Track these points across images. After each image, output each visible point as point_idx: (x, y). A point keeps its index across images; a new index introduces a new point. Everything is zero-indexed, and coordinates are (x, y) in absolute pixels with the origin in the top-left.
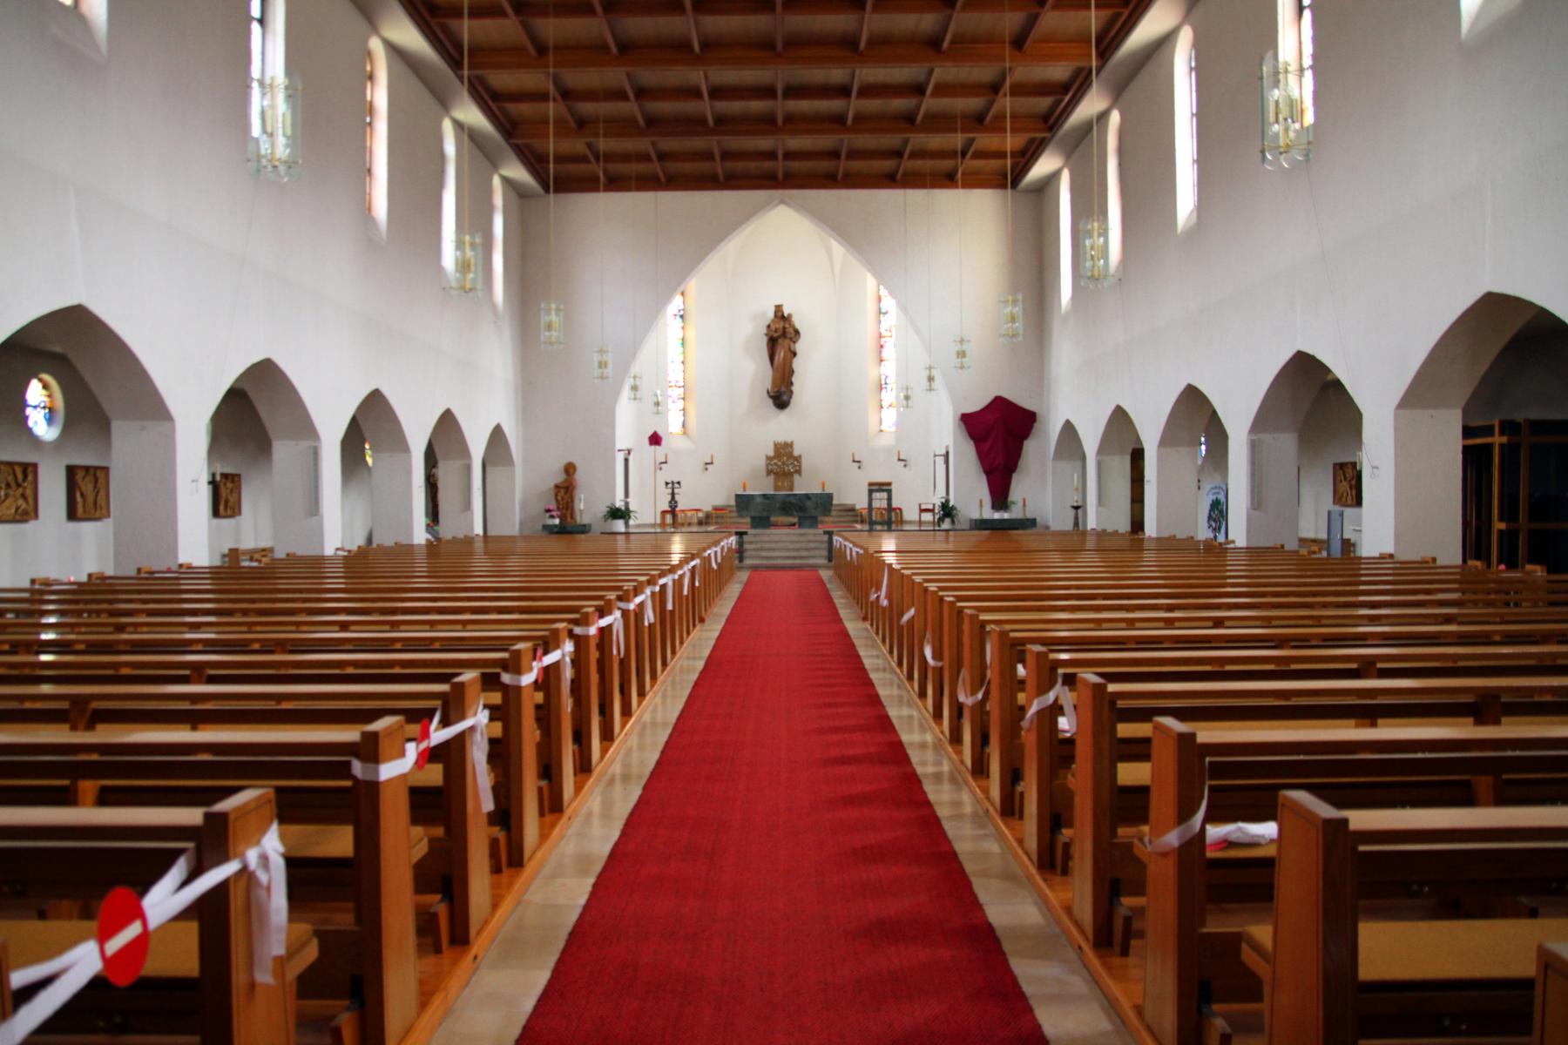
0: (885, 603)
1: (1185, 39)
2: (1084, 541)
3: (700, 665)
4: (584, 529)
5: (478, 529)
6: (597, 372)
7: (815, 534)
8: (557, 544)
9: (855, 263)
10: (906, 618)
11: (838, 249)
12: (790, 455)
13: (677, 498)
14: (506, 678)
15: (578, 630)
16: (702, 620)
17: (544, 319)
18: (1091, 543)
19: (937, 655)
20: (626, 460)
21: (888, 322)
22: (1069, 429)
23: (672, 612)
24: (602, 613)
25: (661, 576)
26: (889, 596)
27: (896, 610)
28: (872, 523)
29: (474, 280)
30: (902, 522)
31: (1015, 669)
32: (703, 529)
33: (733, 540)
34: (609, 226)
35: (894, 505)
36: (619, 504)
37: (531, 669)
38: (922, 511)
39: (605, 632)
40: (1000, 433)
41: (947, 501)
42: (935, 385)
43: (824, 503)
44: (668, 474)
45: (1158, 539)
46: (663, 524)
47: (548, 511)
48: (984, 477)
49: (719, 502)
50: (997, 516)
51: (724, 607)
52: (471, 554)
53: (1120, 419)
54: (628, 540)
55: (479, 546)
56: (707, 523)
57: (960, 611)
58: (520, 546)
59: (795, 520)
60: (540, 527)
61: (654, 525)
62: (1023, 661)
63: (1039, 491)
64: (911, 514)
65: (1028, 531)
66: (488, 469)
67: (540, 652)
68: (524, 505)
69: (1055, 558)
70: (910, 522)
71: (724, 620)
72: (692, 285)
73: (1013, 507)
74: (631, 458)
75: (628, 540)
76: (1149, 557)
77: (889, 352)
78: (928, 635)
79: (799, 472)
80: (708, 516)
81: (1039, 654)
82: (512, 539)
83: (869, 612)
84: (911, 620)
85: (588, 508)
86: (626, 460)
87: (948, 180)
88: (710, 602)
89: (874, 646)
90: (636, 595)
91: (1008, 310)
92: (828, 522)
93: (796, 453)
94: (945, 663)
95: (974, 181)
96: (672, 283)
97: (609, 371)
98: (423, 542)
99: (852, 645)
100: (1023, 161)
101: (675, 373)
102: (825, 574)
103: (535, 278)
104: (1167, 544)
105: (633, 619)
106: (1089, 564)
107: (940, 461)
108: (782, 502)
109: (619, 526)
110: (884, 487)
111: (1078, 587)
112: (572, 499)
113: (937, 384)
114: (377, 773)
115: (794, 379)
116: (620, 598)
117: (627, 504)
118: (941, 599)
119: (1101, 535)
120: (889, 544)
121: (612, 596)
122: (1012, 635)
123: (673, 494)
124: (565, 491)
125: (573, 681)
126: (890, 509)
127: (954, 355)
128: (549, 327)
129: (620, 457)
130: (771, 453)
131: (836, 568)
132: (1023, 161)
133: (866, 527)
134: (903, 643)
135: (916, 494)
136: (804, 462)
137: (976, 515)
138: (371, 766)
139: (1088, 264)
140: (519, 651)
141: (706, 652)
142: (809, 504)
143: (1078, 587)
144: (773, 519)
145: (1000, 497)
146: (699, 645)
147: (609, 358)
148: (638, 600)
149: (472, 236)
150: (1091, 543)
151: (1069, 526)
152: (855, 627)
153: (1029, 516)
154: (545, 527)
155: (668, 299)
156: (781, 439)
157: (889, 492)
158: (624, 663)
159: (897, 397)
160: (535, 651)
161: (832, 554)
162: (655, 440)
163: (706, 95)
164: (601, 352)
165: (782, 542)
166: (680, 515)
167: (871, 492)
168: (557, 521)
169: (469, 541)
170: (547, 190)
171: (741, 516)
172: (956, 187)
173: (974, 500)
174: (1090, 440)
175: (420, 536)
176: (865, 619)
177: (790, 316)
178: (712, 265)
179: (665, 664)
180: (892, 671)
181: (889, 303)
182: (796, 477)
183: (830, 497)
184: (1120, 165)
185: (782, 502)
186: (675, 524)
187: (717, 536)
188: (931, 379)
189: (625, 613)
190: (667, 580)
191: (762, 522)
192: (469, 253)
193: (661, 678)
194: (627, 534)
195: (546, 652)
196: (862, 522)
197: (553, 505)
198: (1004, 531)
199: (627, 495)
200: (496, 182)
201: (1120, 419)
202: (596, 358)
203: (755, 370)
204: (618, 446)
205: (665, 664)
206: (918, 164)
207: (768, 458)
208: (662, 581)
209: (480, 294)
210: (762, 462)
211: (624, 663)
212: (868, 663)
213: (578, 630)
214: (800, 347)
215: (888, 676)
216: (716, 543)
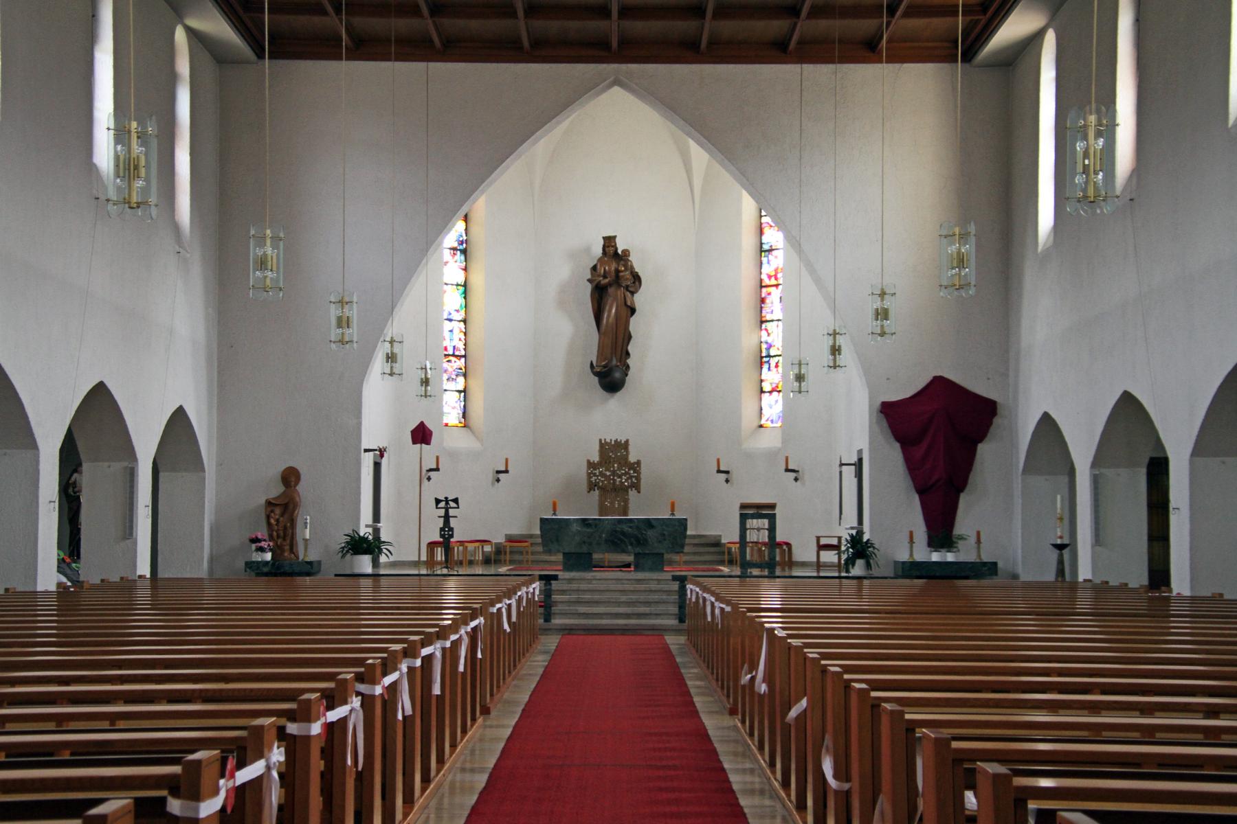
0: (763, 688)
1: (1050, 39)
2: (1073, 599)
3: (481, 780)
4: (310, 569)
5: (144, 568)
6: (335, 333)
7: (660, 580)
8: (265, 591)
9: (725, 178)
10: (793, 713)
11: (699, 155)
12: (624, 461)
13: (453, 522)
14: (175, 806)
15: (292, 728)
16: (486, 711)
17: (255, 252)
18: (1084, 602)
19: (842, 772)
20: (377, 466)
21: (774, 262)
22: (1047, 424)
23: (440, 698)
24: (332, 700)
25: (424, 644)
26: (768, 679)
27: (779, 701)
28: (745, 565)
29: (145, 191)
30: (791, 564)
31: (962, 799)
32: (492, 570)
33: (536, 586)
34: (355, 110)
35: (778, 539)
36: (364, 531)
37: (216, 792)
38: (822, 547)
39: (335, 730)
40: (940, 432)
41: (860, 533)
42: (842, 359)
43: (673, 533)
44: (439, 487)
45: (1193, 599)
46: (431, 563)
47: (255, 540)
48: (916, 499)
49: (515, 531)
50: (935, 557)
51: (518, 693)
52: (130, 606)
53: (1128, 409)
54: (376, 587)
55: (143, 595)
56: (498, 562)
57: (876, 705)
58: (209, 595)
59: (630, 558)
60: (241, 564)
61: (416, 564)
62: (972, 787)
63: (1000, 519)
64: (804, 552)
65: (985, 582)
66: (163, 476)
67: (230, 765)
68: (216, 530)
69: (1028, 624)
70: (803, 564)
71: (519, 710)
72: (480, 205)
73: (961, 544)
74: (384, 462)
75: (376, 587)
76: (1180, 627)
77: (774, 308)
78: (828, 740)
79: (636, 486)
80: (499, 550)
81: (996, 776)
82: (196, 583)
83: (738, 701)
84: (803, 715)
85: (316, 536)
86: (377, 466)
87: (867, 50)
88: (497, 686)
89: (746, 754)
90: (385, 674)
91: (953, 249)
92: (679, 564)
93: (632, 459)
94: (854, 785)
95: (907, 51)
96: (454, 202)
97: (353, 332)
98: (53, 588)
99: (714, 753)
100: (983, 19)
101: (453, 337)
102: (674, 642)
103: (244, 197)
104: (1208, 608)
105: (379, 711)
106: (1082, 635)
107: (849, 472)
108: (611, 528)
109: (364, 564)
110: (765, 511)
111: (1060, 673)
112: (293, 522)
113: (847, 357)
114: (197, 810)
115: (631, 348)
116: (360, 678)
117: (377, 531)
118: (847, 685)
119: (1100, 589)
120: (771, 596)
121: (348, 674)
122: (955, 745)
123: (447, 517)
124: (282, 510)
125: (281, 808)
126: (773, 543)
127: (870, 314)
128: (262, 264)
129: (368, 461)
130: (596, 458)
131: (689, 633)
132: (983, 19)
133: (737, 571)
134: (791, 750)
135: (814, 521)
136: (644, 470)
137: (904, 556)
138: (193, 804)
139: (1079, 179)
140: (198, 763)
141: (491, 763)
142: (650, 533)
143: (1060, 673)
144: (596, 556)
145: (941, 529)
146: (484, 744)
147: (353, 313)
148: (388, 680)
149: (141, 123)
150: (1084, 602)
151: (1050, 576)
152: (716, 724)
153: (986, 558)
154: (250, 565)
155: (443, 226)
156: (610, 437)
157: (772, 519)
158: (363, 779)
159: (784, 377)
160: (224, 761)
161: (685, 611)
162: (421, 435)
163: (521, 13)
164: (342, 303)
165: (610, 592)
166: (457, 551)
167: (743, 518)
168: (268, 556)
169: (128, 585)
170: (260, 55)
171: (549, 552)
172: (881, 62)
173: (902, 533)
174: (1082, 448)
175: (48, 578)
176: (733, 712)
177: (626, 253)
178: (510, 177)
179: (426, 780)
180: (774, 795)
181: (773, 237)
182: (632, 493)
183: (683, 523)
184: (1138, 21)
185: (611, 528)
186: (448, 563)
187: (513, 581)
188: (835, 350)
189: (367, 701)
190: (433, 649)
191: (580, 561)
192: (137, 149)
193: (419, 802)
194: (375, 576)
195: (241, 765)
196: (731, 562)
197: (262, 533)
198: (947, 582)
199: (376, 516)
200: (180, 35)
201: (1128, 409)
202: (334, 312)
203: (570, 333)
204: (365, 445)
205: (426, 780)
206: (823, 25)
207: (590, 465)
208: (425, 651)
209: (154, 211)
210: (583, 471)
211: (363, 779)
212: (736, 781)
213: (292, 728)
214: (639, 299)
215: (767, 802)
216: (509, 593)
